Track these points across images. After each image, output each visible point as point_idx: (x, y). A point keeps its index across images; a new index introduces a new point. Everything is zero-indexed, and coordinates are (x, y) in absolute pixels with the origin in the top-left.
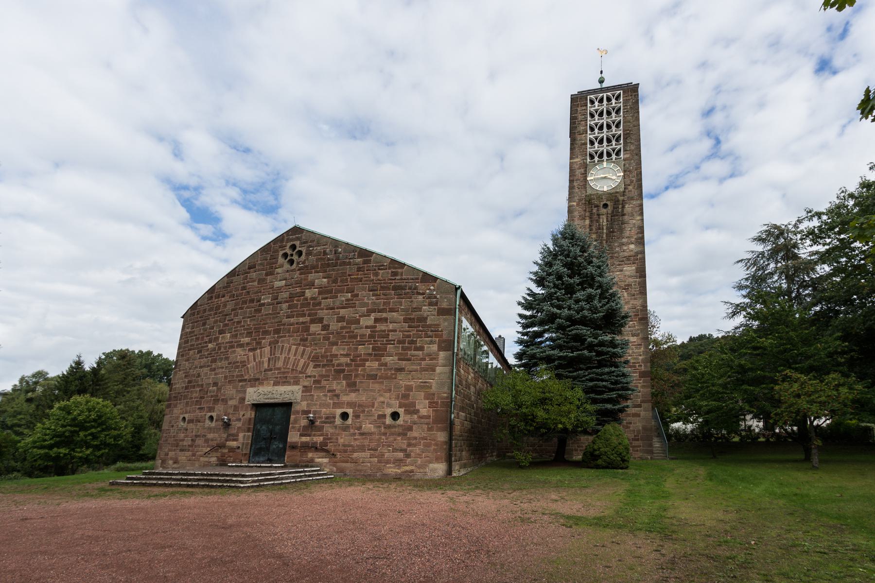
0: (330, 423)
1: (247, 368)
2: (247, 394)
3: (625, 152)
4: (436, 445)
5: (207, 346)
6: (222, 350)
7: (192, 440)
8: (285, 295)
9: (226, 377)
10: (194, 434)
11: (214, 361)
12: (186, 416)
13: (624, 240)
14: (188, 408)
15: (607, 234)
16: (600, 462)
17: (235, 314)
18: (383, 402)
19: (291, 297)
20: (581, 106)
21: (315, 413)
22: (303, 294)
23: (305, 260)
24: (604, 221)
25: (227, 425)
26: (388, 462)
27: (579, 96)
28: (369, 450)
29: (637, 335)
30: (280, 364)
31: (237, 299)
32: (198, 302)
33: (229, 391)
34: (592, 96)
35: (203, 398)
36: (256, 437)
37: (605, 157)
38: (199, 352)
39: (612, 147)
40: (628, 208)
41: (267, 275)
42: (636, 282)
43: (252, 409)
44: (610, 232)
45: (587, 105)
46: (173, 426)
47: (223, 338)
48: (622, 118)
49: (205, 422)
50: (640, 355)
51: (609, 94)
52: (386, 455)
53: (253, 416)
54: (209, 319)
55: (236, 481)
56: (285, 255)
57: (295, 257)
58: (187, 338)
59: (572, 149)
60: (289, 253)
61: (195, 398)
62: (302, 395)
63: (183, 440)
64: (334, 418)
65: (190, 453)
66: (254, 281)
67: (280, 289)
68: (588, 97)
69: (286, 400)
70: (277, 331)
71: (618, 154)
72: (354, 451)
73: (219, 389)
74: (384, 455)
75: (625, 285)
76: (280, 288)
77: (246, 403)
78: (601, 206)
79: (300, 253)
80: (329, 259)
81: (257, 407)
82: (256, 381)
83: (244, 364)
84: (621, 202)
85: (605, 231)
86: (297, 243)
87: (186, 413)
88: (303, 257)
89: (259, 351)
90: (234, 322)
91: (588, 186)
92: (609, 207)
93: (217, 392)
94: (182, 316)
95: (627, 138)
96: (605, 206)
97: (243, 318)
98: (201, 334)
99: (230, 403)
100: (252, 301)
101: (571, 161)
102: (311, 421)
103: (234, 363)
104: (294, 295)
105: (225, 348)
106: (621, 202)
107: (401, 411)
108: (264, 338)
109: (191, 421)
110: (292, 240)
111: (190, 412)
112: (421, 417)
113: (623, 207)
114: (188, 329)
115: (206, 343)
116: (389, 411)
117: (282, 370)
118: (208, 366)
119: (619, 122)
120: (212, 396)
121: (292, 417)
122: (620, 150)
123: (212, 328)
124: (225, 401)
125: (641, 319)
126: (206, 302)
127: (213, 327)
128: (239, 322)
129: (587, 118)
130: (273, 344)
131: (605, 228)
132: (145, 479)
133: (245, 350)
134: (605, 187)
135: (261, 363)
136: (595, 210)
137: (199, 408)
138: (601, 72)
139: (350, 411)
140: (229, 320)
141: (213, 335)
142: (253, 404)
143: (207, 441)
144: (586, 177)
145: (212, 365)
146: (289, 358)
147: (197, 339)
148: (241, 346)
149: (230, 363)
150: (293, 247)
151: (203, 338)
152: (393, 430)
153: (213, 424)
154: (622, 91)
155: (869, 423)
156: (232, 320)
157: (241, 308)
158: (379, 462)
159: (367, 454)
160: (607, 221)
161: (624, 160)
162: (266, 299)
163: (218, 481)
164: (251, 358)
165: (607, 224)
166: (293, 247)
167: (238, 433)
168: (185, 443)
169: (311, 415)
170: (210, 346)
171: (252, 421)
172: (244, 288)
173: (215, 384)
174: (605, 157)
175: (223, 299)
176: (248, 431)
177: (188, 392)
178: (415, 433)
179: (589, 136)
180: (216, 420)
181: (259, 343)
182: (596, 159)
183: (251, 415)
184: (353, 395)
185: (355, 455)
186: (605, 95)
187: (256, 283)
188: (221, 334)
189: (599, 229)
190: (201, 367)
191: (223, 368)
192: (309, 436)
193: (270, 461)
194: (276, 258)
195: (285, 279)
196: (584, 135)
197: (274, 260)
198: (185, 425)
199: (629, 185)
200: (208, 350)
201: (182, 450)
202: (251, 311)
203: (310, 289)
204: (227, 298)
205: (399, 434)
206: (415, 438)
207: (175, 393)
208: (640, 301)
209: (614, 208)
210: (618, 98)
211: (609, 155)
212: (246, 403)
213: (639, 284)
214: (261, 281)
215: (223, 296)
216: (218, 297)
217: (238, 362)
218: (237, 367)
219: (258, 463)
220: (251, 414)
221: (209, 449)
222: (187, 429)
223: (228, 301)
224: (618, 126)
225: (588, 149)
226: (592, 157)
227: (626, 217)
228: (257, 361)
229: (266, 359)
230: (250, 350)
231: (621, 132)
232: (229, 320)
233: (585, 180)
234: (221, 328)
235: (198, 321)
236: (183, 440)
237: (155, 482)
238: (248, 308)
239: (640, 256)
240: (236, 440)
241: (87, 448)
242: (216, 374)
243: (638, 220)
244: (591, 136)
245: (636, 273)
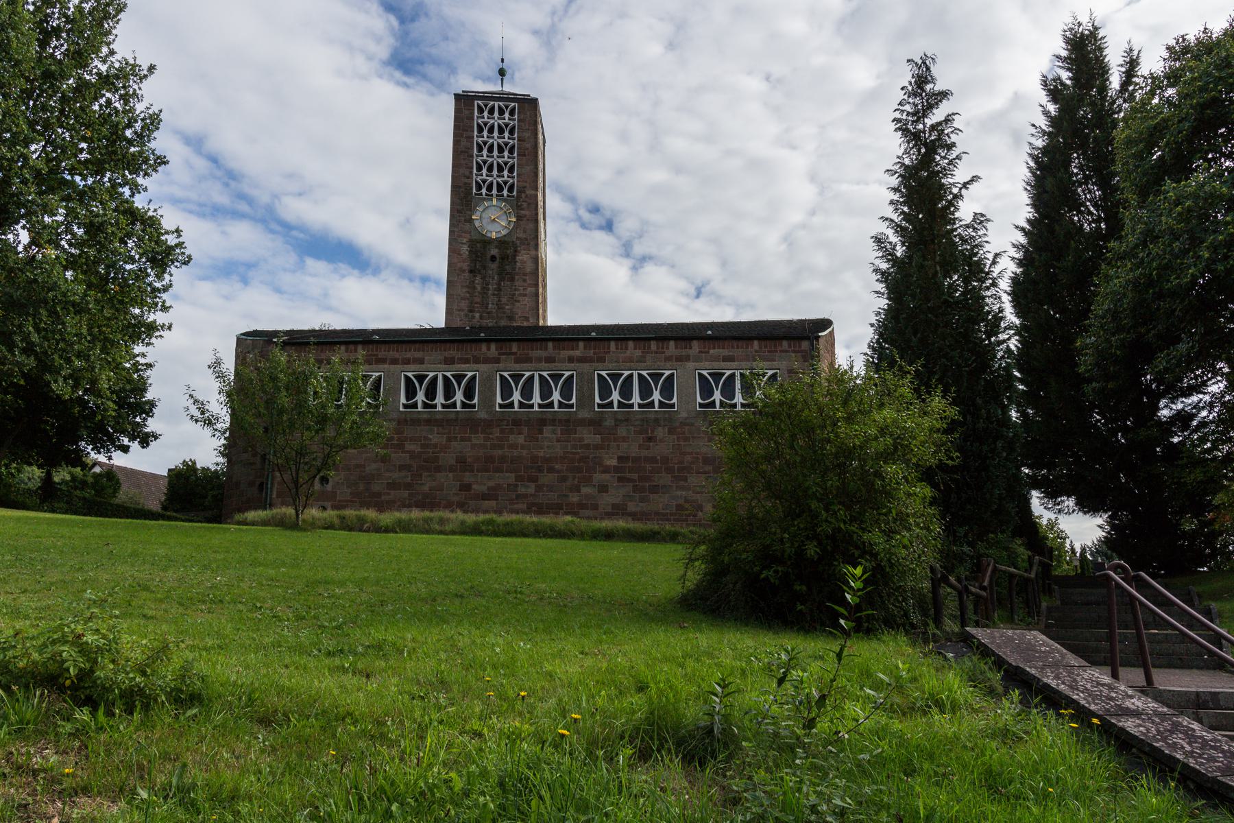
37: (495, 191)
76: (98, 272)
119: (513, 147)
134: (494, 234)
174: (495, 191)
182: (484, 191)
186: (496, 104)
211: (500, 188)
225: (474, 177)
241: (764, 472)
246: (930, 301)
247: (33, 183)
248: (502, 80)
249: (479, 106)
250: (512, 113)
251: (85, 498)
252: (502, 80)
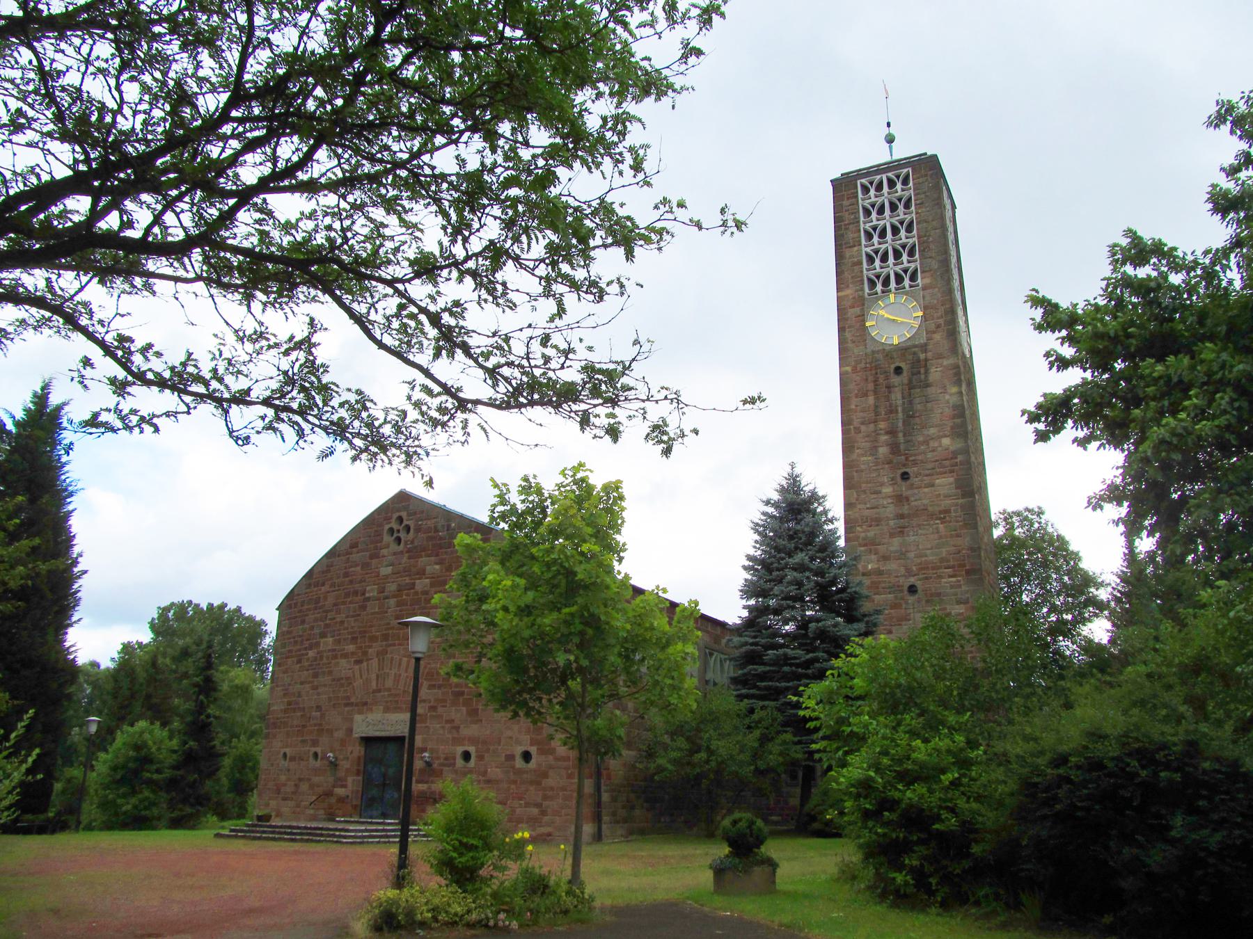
0: (449, 765)
5: (307, 654)
6: (325, 661)
7: (296, 785)
9: (330, 699)
11: (316, 676)
12: (288, 750)
13: (932, 431)
16: (816, 826)
18: (511, 738)
20: (848, 199)
21: (432, 751)
22: (413, 586)
24: (897, 397)
25: (334, 765)
29: (966, 602)
30: (389, 683)
34: (863, 181)
36: (367, 783)
37: (893, 285)
38: (299, 661)
39: (902, 266)
40: (935, 374)
41: (371, 557)
42: (957, 505)
44: (909, 417)
46: (272, 765)
48: (914, 215)
51: (890, 174)
53: (363, 753)
54: (307, 615)
57: (402, 535)
64: (454, 759)
66: (357, 565)
68: (859, 182)
70: (385, 637)
71: (913, 277)
73: (323, 716)
75: (940, 512)
76: (387, 577)
78: (892, 371)
79: (408, 529)
80: (441, 538)
81: (368, 741)
82: (364, 706)
84: (922, 363)
85: (900, 415)
86: (404, 514)
89: (365, 664)
92: (905, 374)
95: (924, 250)
96: (898, 370)
97: (347, 617)
99: (336, 734)
100: (356, 593)
103: (339, 680)
106: (922, 363)
107: (533, 750)
108: (370, 647)
110: (399, 511)
112: (557, 759)
113: (927, 372)
115: (306, 649)
116: (519, 750)
117: (393, 692)
118: (309, 682)
119: (911, 223)
120: (315, 725)
122: (916, 271)
123: (312, 628)
124: (330, 732)
128: (342, 622)
130: (382, 654)
131: (900, 409)
138: (889, 125)
139: (472, 749)
140: (330, 619)
144: (864, 321)
146: (400, 675)
148: (345, 656)
149: (334, 680)
150: (400, 520)
151: (302, 641)
152: (525, 776)
154: (910, 169)
157: (344, 603)
160: (903, 398)
161: (924, 288)
162: (372, 591)
165: (904, 403)
166: (400, 520)
169: (426, 754)
171: (362, 761)
172: (346, 575)
173: (319, 708)
174: (893, 285)
178: (549, 782)
179: (864, 250)
180: (322, 759)
181: (365, 653)
182: (879, 288)
184: (475, 727)
187: (359, 568)
189: (891, 412)
190: (302, 683)
192: (427, 782)
193: (384, 816)
196: (856, 249)
201: (285, 799)
205: (531, 783)
206: (552, 789)
209: (913, 374)
210: (905, 182)
211: (899, 279)
214: (365, 565)
218: (342, 685)
219: (371, 818)
221: (314, 798)
224: (909, 229)
225: (865, 272)
226: (872, 284)
227: (931, 391)
229: (374, 676)
231: (915, 239)
233: (864, 328)
238: (350, 603)
239: (960, 458)
243: (954, 394)
244: (868, 250)
245: (956, 488)
246: (528, 669)
248: (890, 148)
249: (863, 186)
250: (905, 182)
252: (890, 148)
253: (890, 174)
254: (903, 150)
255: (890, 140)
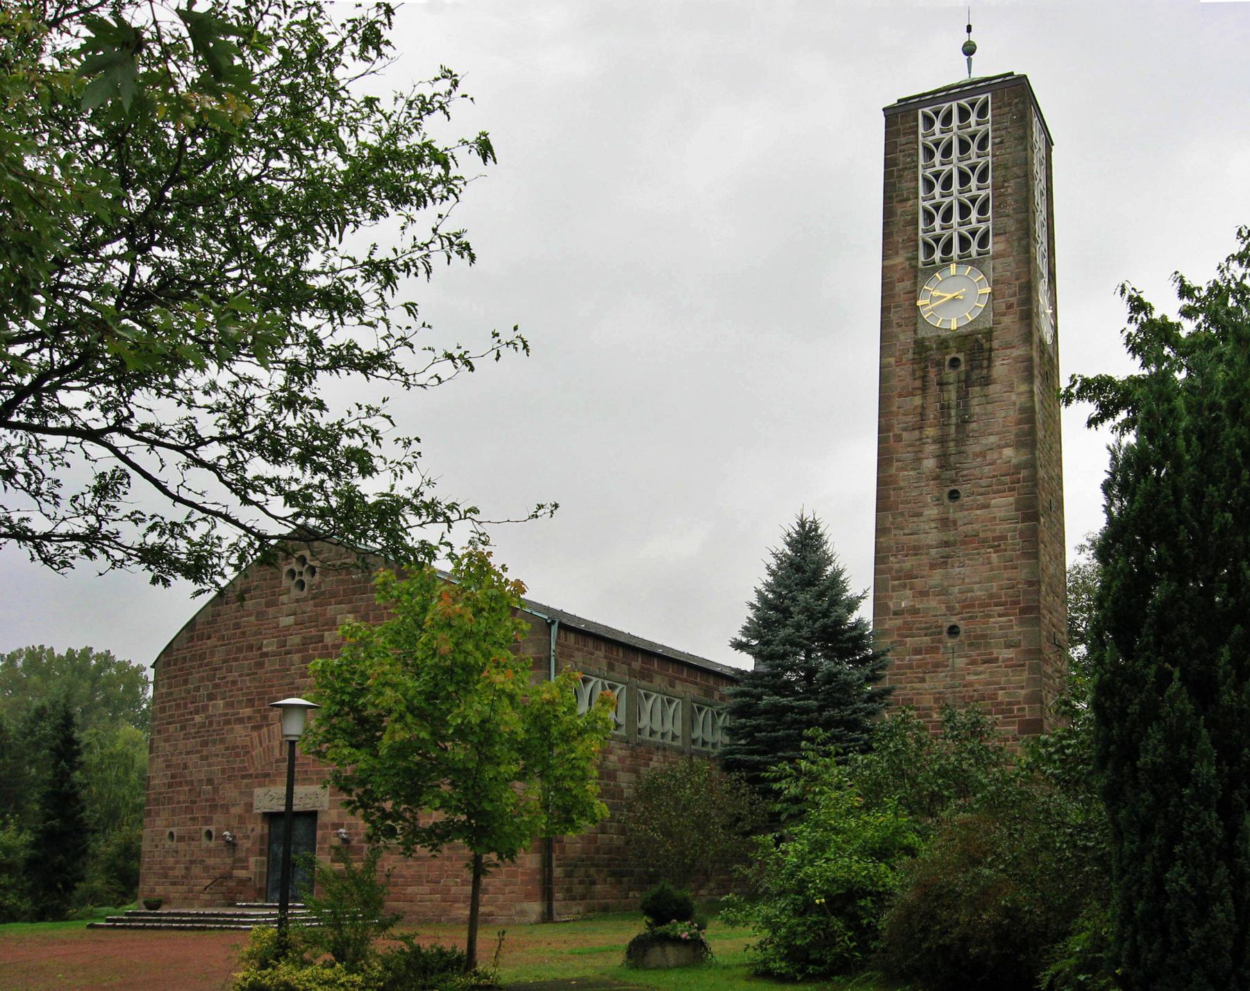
1: (252, 756)
2: (255, 798)
3: (997, 239)
4: (523, 874)
5: (193, 719)
6: (215, 726)
8: (295, 640)
10: (187, 858)
12: (174, 830)
14: (176, 818)
15: (957, 426)
17: (227, 669)
19: (305, 643)
20: (905, 134)
23: (320, 583)
25: (232, 845)
26: (456, 900)
27: (900, 110)
28: (427, 882)
31: (229, 644)
32: (174, 645)
33: (230, 792)
34: (927, 110)
35: (195, 802)
37: (956, 251)
38: (183, 728)
41: (268, 605)
43: (263, 821)
45: (916, 133)
46: (157, 846)
47: (214, 706)
49: (200, 840)
50: (1022, 688)
51: (962, 102)
52: (453, 890)
53: (266, 831)
54: (191, 674)
55: (238, 922)
56: (292, 573)
57: (306, 578)
58: (163, 703)
59: (887, 236)
60: (297, 570)
61: (184, 802)
62: (330, 801)
63: (173, 868)
65: (185, 887)
67: (288, 630)
68: (920, 112)
69: (309, 808)
71: (983, 242)
72: (406, 885)
73: (216, 790)
74: (450, 890)
76: (288, 628)
77: (256, 811)
78: (947, 363)
79: (312, 571)
83: (247, 751)
87: (174, 826)
88: (317, 576)
89: (265, 730)
90: (227, 682)
91: (920, 320)
93: (214, 793)
94: (151, 664)
97: (240, 676)
98: (183, 698)
100: (250, 648)
101: (887, 263)
102: (344, 839)
103: (234, 748)
104: (309, 641)
105: (219, 723)
109: (181, 839)
111: (178, 825)
114: (163, 687)
118: (198, 752)
120: (207, 800)
121: (319, 833)
123: (197, 689)
124: (226, 808)
125: (1024, 611)
126: (185, 646)
127: (199, 687)
128: (234, 683)
129: (917, 161)
132: (129, 921)
133: (247, 728)
135: (270, 749)
136: (932, 372)
137: (191, 819)
138: (969, 29)
140: (219, 679)
141: (200, 701)
142: (264, 814)
143: (207, 869)
144: (916, 299)
145: (202, 751)
147: (178, 706)
148: (240, 721)
149: (227, 749)
151: (185, 705)
153: (212, 844)
154: (989, 95)
155: (211, 906)
156: (225, 678)
157: (236, 659)
158: (444, 900)
159: (426, 888)
162: (270, 646)
163: (217, 922)
164: (256, 741)
167: (247, 857)
168: (177, 873)
170: (198, 719)
171: (266, 840)
172: (237, 626)
173: (210, 781)
174: (956, 251)
175: (209, 642)
176: (261, 855)
177: (173, 792)
179: (921, 204)
182: (938, 255)
183: (262, 830)
185: (410, 890)
186: (954, 105)
187: (253, 618)
188: (211, 700)
190: (188, 753)
191: (217, 755)
194: (279, 578)
195: (294, 614)
196: (910, 203)
197: (275, 581)
198: (174, 844)
199: (1004, 315)
200: (195, 725)
201: (174, 884)
202: (250, 664)
203: (330, 630)
204: (212, 642)
207: (154, 793)
208: (1024, 571)
210: (982, 113)
212: (256, 811)
213: (1022, 533)
214: (260, 615)
215: (209, 638)
216: (201, 638)
217: (238, 747)
218: (238, 755)
220: (262, 827)
221: (210, 881)
222: (177, 852)
223: (216, 646)
225: (920, 233)
226: (929, 250)
228: (264, 745)
230: (254, 728)
232: (219, 679)
234: (210, 691)
235: (176, 676)
236: (173, 868)
237: (141, 924)
238: (245, 658)
240: (246, 868)
242: (210, 765)
247: (274, 968)
248: (969, 62)
249: (926, 116)
250: (982, 113)
251: (272, 68)
252: (969, 62)
253: (962, 102)
254: (987, 66)
255: (969, 50)
